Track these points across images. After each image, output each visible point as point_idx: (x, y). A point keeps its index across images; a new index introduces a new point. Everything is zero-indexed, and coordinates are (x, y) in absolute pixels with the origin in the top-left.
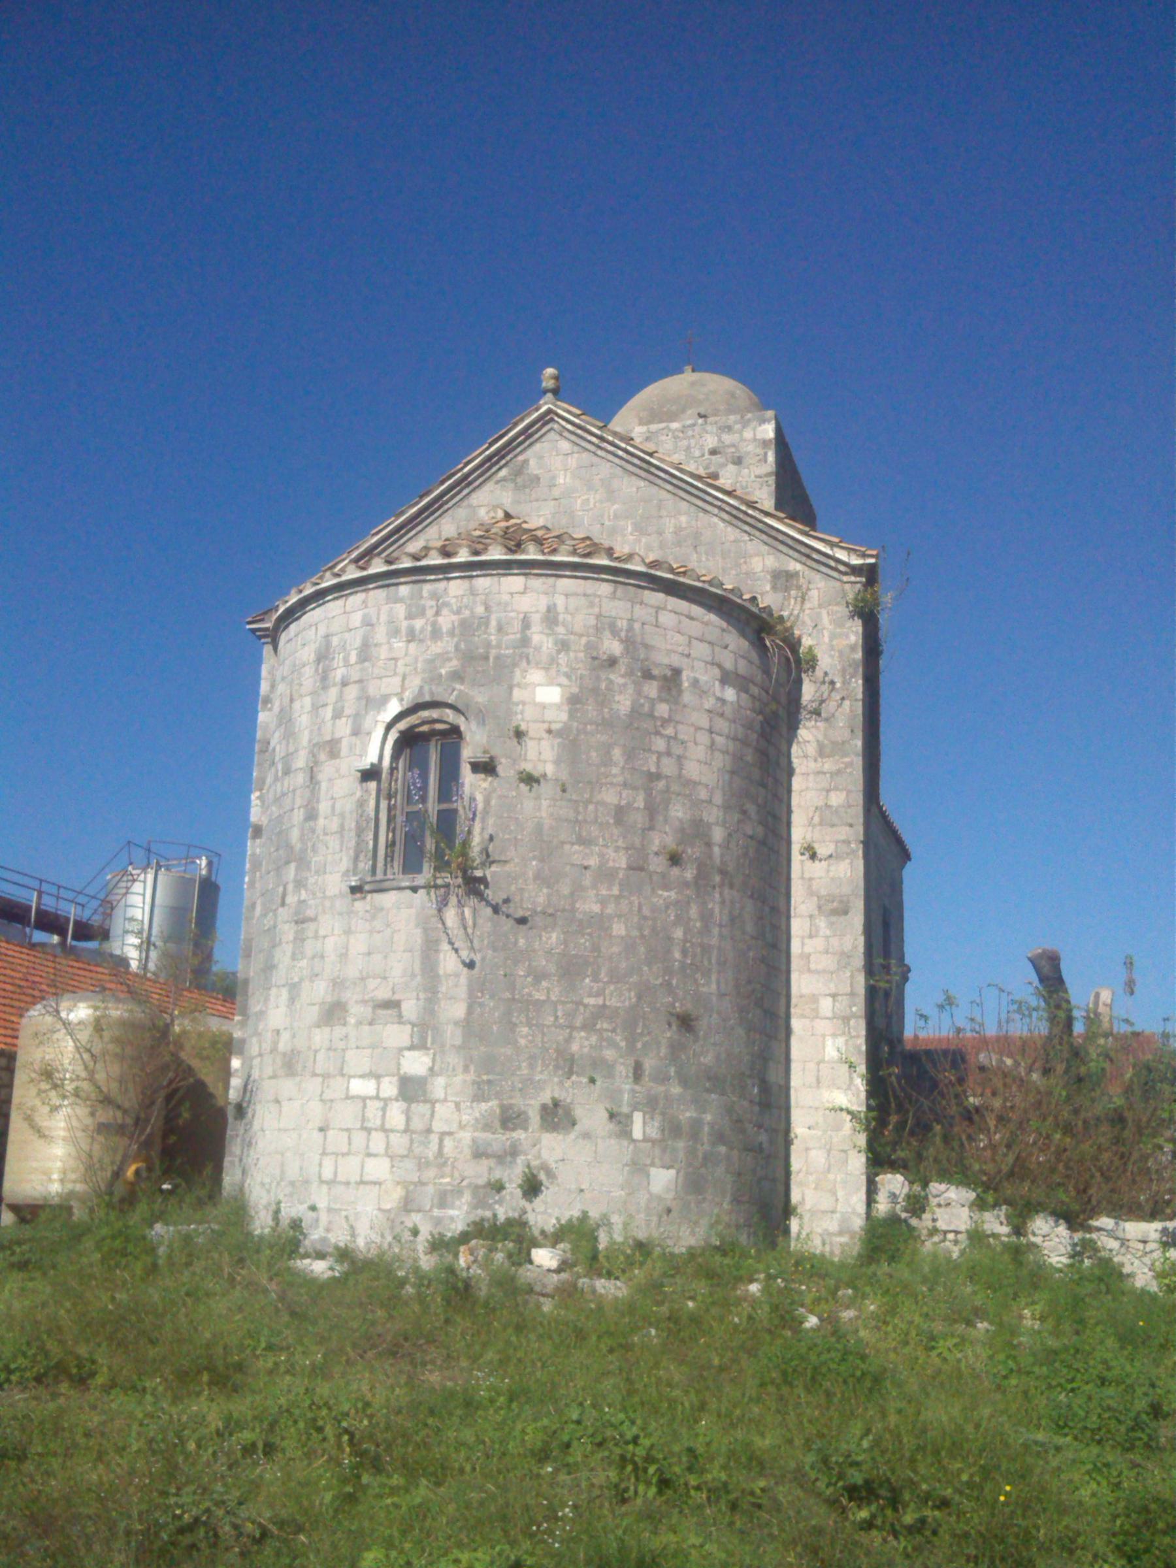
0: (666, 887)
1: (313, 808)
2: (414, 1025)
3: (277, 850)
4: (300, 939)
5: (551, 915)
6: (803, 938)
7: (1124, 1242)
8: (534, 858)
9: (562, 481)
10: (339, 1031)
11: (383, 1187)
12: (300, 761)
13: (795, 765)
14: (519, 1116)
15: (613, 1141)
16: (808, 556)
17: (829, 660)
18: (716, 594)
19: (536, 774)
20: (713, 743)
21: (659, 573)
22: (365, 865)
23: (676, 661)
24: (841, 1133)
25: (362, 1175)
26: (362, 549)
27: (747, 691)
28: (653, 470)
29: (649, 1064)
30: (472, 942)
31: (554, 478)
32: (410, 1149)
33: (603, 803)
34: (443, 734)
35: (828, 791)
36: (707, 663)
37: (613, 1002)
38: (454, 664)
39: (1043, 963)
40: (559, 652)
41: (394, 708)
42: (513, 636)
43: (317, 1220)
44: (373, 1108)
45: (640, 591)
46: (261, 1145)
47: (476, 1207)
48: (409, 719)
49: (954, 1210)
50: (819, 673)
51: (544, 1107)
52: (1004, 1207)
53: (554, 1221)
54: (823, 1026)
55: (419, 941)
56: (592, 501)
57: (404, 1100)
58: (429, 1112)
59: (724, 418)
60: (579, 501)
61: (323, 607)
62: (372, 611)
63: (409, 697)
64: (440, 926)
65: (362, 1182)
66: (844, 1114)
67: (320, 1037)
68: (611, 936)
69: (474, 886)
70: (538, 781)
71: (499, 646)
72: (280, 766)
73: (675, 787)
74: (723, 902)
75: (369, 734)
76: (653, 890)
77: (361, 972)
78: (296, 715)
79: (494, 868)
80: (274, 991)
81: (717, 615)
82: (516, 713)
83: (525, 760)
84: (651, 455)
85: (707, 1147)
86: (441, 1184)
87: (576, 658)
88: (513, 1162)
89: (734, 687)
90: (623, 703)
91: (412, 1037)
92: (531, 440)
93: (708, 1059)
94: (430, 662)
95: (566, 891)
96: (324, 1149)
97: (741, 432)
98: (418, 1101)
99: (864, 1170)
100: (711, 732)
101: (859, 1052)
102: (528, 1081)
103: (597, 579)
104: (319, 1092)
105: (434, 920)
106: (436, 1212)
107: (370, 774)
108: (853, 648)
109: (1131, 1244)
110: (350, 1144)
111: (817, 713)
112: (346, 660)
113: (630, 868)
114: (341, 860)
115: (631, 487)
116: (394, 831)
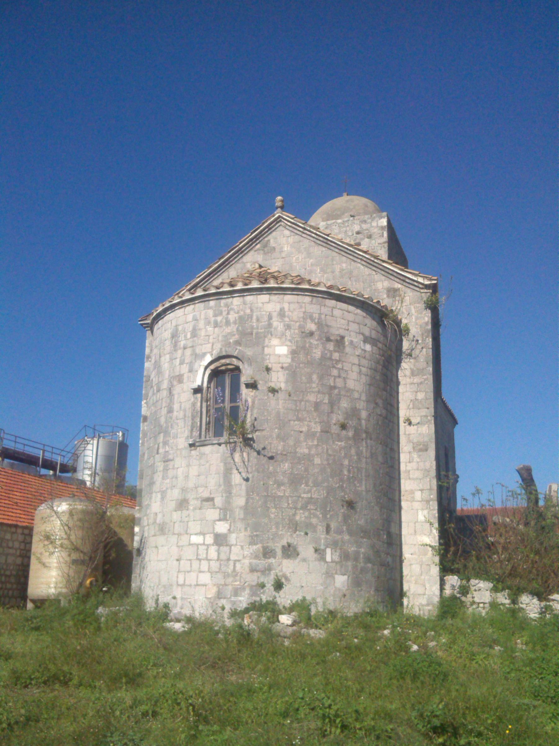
2: (220, 509)
3: (154, 427)
4: (166, 470)
5: (285, 455)
8: (276, 428)
9: (286, 249)
10: (185, 513)
11: (207, 587)
12: (165, 385)
13: (400, 380)
14: (271, 552)
15: (317, 563)
16: (404, 281)
19: (276, 388)
21: (333, 291)
22: (196, 434)
23: (342, 332)
25: (197, 581)
26: (192, 285)
27: (376, 346)
28: (329, 243)
29: (333, 525)
31: (282, 248)
32: (220, 569)
34: (232, 370)
35: (416, 392)
36: (357, 333)
37: (315, 496)
38: (237, 337)
39: (523, 472)
40: (286, 330)
41: (208, 359)
45: (324, 300)
46: (149, 569)
47: (252, 596)
49: (483, 593)
50: (411, 336)
51: (283, 547)
52: (507, 590)
53: (289, 602)
54: (416, 505)
55: (222, 469)
56: (300, 258)
58: (229, 551)
60: (294, 258)
62: (197, 314)
63: (215, 353)
64: (232, 461)
65: (197, 585)
66: (428, 547)
67: (176, 516)
69: (248, 442)
70: (277, 391)
71: (257, 328)
72: (155, 388)
73: (343, 393)
74: (367, 447)
75: (197, 371)
76: (333, 443)
77: (195, 484)
80: (154, 495)
82: (266, 360)
83: (271, 381)
84: (328, 235)
86: (235, 585)
87: (294, 333)
88: (270, 574)
90: (317, 353)
91: (220, 515)
93: (362, 522)
94: (225, 336)
96: (179, 569)
97: (371, 223)
99: (438, 574)
100: (359, 365)
101: (435, 518)
102: (275, 535)
103: (304, 295)
106: (233, 599)
107: (198, 390)
108: (427, 324)
110: (191, 567)
111: (410, 355)
112: (185, 336)
114: (185, 431)
115: (319, 251)
116: (209, 417)
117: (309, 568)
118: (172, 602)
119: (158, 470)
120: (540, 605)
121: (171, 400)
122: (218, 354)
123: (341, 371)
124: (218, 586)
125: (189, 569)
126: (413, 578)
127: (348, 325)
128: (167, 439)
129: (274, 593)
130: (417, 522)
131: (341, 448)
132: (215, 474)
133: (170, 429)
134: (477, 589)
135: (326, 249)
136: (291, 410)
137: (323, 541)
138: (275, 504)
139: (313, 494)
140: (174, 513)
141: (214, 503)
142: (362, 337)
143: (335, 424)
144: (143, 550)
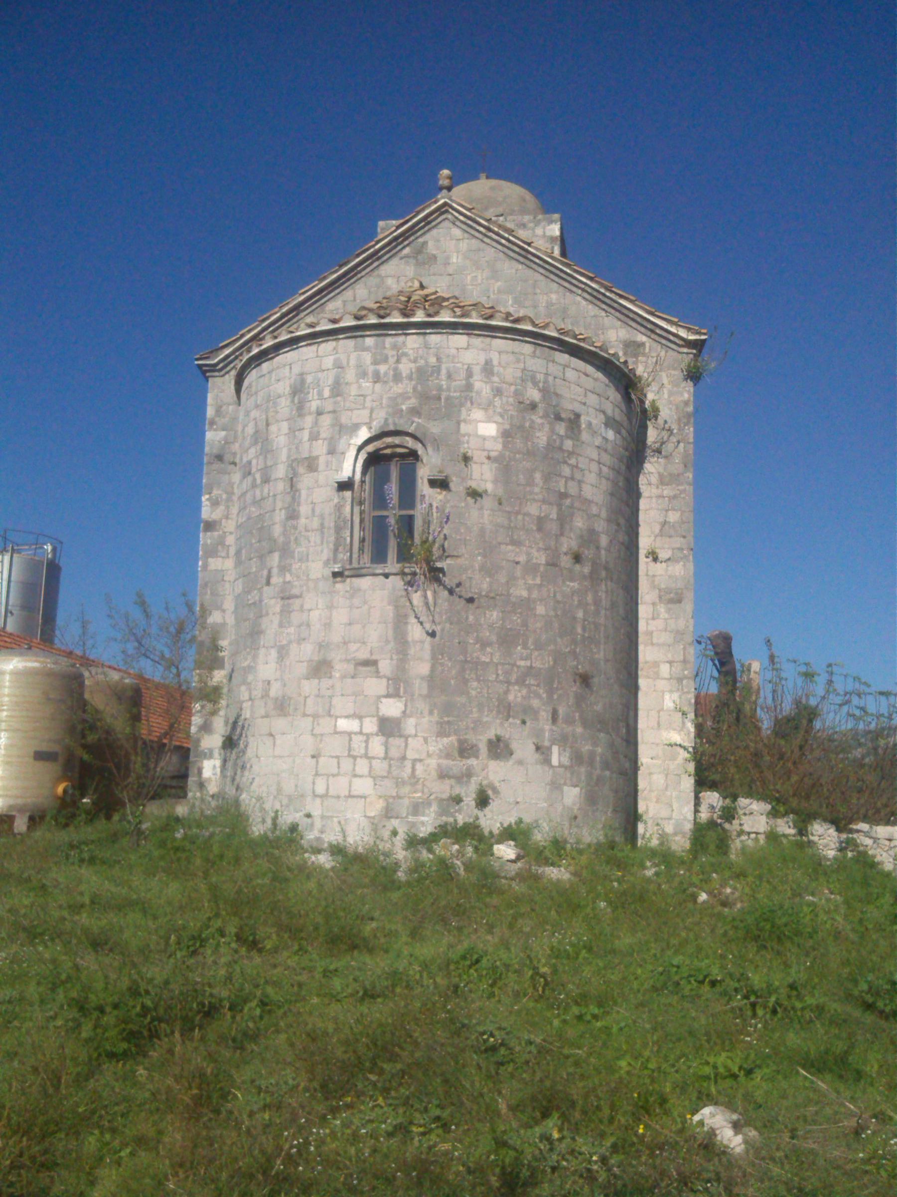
0: (572, 580)
1: (294, 510)
2: (389, 679)
3: (259, 541)
4: (286, 612)
5: (493, 598)
6: (647, 619)
7: (876, 840)
8: (479, 554)
9: (455, 260)
10: (325, 683)
11: (368, 800)
12: (281, 471)
13: (642, 491)
14: (472, 747)
15: (539, 767)
16: (652, 331)
17: (668, 412)
18: (603, 357)
19: (480, 490)
20: (600, 469)
21: (567, 339)
22: (343, 556)
23: (578, 408)
24: (676, 762)
25: (350, 791)
26: (291, 305)
27: (619, 433)
28: (530, 256)
29: (561, 711)
30: (433, 616)
31: (448, 258)
32: (389, 772)
33: (527, 514)
34: (402, 456)
35: (667, 511)
36: (596, 410)
37: (538, 664)
38: (413, 402)
39: (719, 641)
40: (495, 396)
41: (364, 434)
42: (460, 382)
43: (312, 825)
44: (358, 741)
45: (552, 352)
46: (256, 768)
47: (441, 815)
48: (375, 443)
49: (756, 818)
50: (660, 421)
51: (490, 742)
52: (791, 816)
53: (498, 825)
54: (662, 684)
55: (391, 615)
56: (480, 277)
57: (383, 735)
58: (404, 744)
59: (520, 217)
60: (469, 278)
61: (296, 351)
62: (343, 357)
63: (377, 426)
64: (408, 604)
65: (350, 796)
66: (679, 749)
67: (309, 687)
68: (535, 615)
69: (435, 574)
70: (480, 496)
71: (448, 389)
72: (258, 476)
73: (577, 504)
74: (607, 592)
75: (343, 453)
76: (564, 582)
77: (343, 638)
78: (272, 436)
79: (449, 561)
80: (262, 652)
81: (604, 375)
82: (464, 443)
83: (471, 479)
84: (529, 244)
85: (598, 772)
86: (414, 798)
87: (507, 402)
88: (469, 782)
89: (613, 430)
90: (541, 438)
91: (388, 688)
92: (430, 226)
93: (599, 708)
94: (393, 399)
95: (503, 580)
96: (317, 771)
97: (533, 229)
98: (394, 736)
99: (693, 789)
100: (599, 463)
101: (690, 704)
102: (478, 723)
103: (522, 341)
104: (310, 728)
105: (403, 599)
106: (411, 819)
107: (345, 486)
108: (686, 403)
109: (880, 841)
110: (339, 767)
111: (659, 451)
112: (320, 394)
113: (548, 564)
114: (322, 551)
115: (511, 268)
116: (364, 530)
117: (527, 774)
118: (303, 822)
119: (271, 612)
120: (839, 837)
121: (293, 498)
122: (381, 427)
123: (575, 469)
124: (386, 798)
125: (335, 771)
126: (654, 794)
127: (585, 396)
128: (288, 561)
129: (476, 811)
130: (662, 709)
131: (573, 593)
132: (379, 623)
133: (293, 545)
134: (747, 812)
135: (524, 267)
136: (502, 526)
137: (547, 734)
138: (476, 674)
139: (534, 661)
140: (305, 683)
141: (377, 669)
142: (602, 416)
143: (565, 554)
144: (239, 739)
